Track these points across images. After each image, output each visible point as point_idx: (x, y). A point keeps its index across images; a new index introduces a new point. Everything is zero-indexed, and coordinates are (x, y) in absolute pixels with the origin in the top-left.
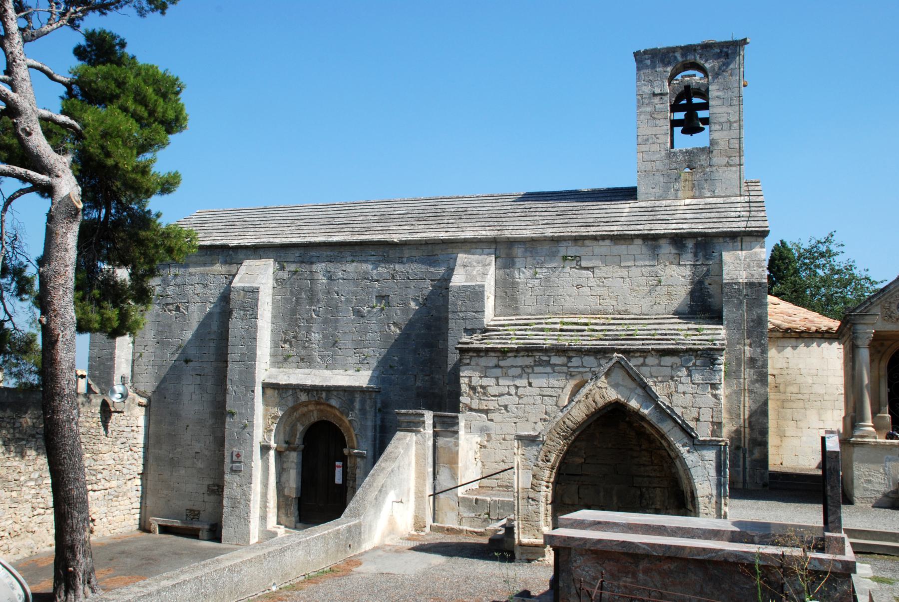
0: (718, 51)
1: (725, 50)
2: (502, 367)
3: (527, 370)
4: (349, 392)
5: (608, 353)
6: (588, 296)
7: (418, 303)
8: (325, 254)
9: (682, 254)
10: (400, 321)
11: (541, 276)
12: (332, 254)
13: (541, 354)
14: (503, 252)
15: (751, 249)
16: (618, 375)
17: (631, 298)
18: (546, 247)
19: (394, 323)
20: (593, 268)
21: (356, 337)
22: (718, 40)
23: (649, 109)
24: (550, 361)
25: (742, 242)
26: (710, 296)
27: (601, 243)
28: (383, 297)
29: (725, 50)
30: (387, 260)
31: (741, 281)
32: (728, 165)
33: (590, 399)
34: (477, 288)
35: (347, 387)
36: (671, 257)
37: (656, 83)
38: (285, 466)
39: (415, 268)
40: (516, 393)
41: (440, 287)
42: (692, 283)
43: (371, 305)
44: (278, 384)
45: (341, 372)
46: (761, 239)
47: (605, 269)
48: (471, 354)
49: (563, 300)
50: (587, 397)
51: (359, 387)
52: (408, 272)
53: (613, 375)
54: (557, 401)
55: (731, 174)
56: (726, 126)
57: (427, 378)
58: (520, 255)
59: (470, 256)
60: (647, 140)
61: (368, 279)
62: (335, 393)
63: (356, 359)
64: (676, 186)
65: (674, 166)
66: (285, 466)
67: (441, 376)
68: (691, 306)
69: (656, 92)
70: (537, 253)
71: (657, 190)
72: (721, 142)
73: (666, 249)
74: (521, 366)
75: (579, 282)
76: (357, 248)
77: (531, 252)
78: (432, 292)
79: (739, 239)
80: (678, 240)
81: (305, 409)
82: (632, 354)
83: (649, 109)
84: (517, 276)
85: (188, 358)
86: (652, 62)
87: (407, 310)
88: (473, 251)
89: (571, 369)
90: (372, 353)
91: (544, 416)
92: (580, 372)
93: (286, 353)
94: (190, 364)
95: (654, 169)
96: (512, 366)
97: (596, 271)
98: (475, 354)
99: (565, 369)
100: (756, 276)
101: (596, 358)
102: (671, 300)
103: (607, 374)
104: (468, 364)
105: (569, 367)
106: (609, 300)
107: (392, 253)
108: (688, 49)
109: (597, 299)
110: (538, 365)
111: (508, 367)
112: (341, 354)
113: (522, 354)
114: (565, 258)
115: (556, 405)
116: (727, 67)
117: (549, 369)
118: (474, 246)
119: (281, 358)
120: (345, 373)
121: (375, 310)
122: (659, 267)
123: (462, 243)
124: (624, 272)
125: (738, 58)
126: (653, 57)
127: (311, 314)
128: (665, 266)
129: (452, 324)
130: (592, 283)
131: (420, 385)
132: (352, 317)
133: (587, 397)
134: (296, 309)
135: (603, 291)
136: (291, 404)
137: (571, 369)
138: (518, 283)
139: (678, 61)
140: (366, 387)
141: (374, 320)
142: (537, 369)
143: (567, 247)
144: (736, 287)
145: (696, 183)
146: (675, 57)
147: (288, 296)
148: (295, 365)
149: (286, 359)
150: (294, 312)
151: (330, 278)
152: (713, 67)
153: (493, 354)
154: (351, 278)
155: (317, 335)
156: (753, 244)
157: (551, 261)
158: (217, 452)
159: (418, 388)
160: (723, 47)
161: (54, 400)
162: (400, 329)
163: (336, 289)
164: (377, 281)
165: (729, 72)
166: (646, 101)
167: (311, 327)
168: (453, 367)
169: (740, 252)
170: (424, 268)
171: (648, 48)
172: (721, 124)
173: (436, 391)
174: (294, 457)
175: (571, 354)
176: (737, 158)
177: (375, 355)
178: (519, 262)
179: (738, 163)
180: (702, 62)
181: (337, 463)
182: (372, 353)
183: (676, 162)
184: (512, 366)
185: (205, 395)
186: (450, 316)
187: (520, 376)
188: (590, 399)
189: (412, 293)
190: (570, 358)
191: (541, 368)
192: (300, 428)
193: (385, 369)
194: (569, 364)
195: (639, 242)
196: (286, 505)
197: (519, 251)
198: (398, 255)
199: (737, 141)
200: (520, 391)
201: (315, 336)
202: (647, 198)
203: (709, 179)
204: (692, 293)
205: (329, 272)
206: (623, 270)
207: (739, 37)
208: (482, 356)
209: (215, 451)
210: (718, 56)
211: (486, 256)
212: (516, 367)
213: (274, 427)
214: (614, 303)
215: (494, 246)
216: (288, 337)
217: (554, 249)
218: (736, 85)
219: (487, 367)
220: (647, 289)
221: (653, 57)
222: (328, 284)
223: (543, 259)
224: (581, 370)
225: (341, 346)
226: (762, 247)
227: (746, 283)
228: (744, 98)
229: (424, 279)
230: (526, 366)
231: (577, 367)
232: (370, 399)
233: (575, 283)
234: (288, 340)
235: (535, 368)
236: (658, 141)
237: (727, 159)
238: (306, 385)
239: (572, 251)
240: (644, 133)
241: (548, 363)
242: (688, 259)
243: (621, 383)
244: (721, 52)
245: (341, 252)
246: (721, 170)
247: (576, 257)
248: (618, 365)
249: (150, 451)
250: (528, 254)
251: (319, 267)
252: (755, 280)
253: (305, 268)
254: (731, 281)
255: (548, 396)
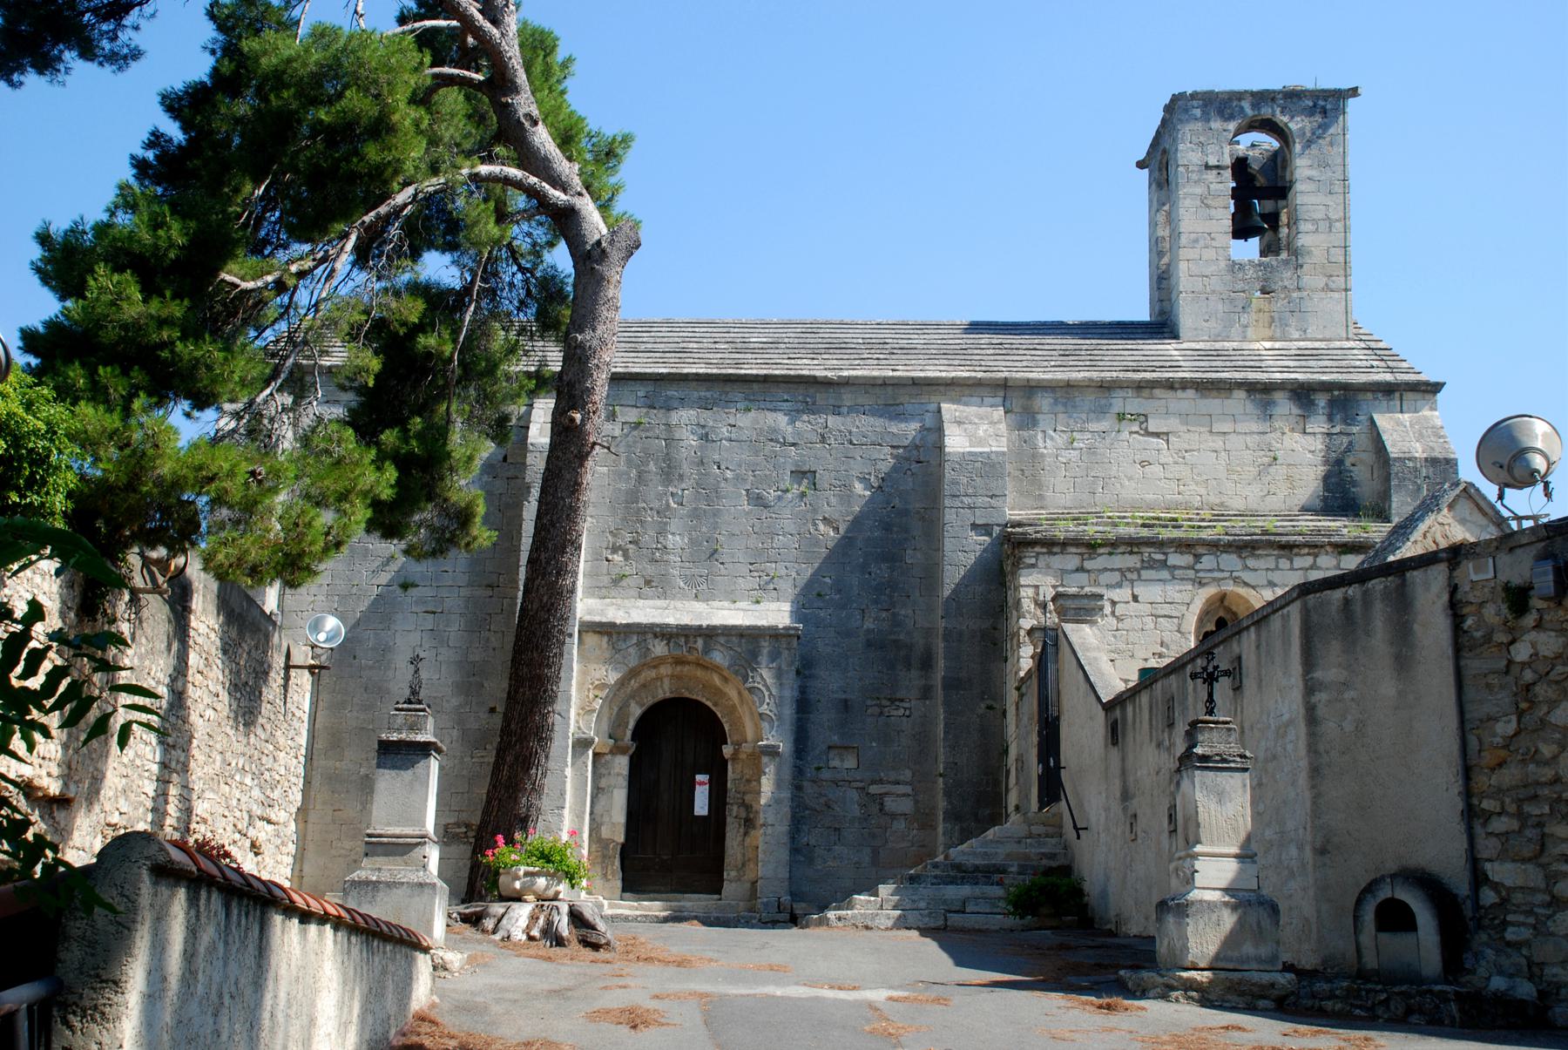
0: (1311, 104)
1: (1321, 103)
2: (1088, 571)
3: (1129, 575)
4: (749, 639)
5: (1259, 549)
6: (1160, 480)
7: (869, 486)
8: (696, 394)
9: (1309, 416)
10: (836, 516)
11: (1082, 445)
12: (708, 394)
13: (1152, 550)
14: (1017, 403)
15: (1416, 411)
16: (1465, 507)
17: (1230, 484)
18: (1090, 398)
19: (825, 519)
20: (1167, 434)
21: (754, 542)
22: (1310, 86)
23: (1199, 190)
24: (1166, 561)
25: (1401, 400)
26: (1354, 483)
27: (1180, 393)
28: (804, 473)
29: (1321, 103)
30: (812, 409)
31: (1417, 455)
32: (1327, 289)
33: (1429, 539)
34: (993, 456)
35: (749, 628)
36: (1293, 419)
37: (1210, 149)
38: (603, 783)
39: (866, 425)
40: (1113, 613)
41: (907, 459)
42: (1326, 462)
43: (782, 487)
44: (612, 625)
45: (726, 604)
46: (1431, 396)
47: (1187, 436)
48: (1038, 549)
49: (1118, 485)
50: (1425, 536)
51: (770, 628)
52: (850, 432)
53: (1458, 507)
54: (1180, 625)
55: (1333, 303)
56: (1323, 226)
57: (884, 615)
58: (1045, 408)
59: (961, 408)
60: (1196, 241)
61: (778, 442)
62: (722, 640)
63: (753, 582)
64: (1244, 319)
65: (1240, 286)
66: (603, 783)
67: (910, 611)
68: (1325, 499)
69: (1210, 164)
70: (1074, 407)
71: (1212, 324)
72: (1316, 252)
73: (1284, 406)
74: (1119, 570)
75: (1145, 456)
76: (755, 386)
77: (1065, 405)
78: (894, 469)
79: (1397, 395)
80: (1303, 394)
81: (653, 674)
82: (1296, 550)
83: (1199, 190)
84: (1041, 444)
85: (410, 580)
86: (1203, 112)
87: (849, 496)
88: (964, 399)
89: (1201, 574)
90: (783, 572)
91: (1159, 649)
92: (1214, 579)
93: (617, 570)
94: (412, 591)
95: (1208, 290)
96: (1106, 570)
97: (1172, 438)
98: (1044, 550)
99: (1191, 573)
100: (1438, 450)
101: (1240, 557)
102: (1293, 488)
103: (1451, 507)
104: (1033, 566)
105: (1197, 571)
106: (1194, 487)
107: (821, 398)
108: (1262, 97)
109: (1174, 485)
110: (1147, 568)
111: (1099, 571)
112: (723, 572)
113: (1121, 549)
114: (1121, 417)
115: (1179, 631)
116: (1325, 131)
117: (1165, 574)
118: (967, 392)
119: (606, 580)
120: (732, 606)
121: (789, 495)
122: (1272, 435)
123: (947, 385)
124: (1218, 443)
125: (1341, 118)
126: (1206, 106)
127: (667, 501)
128: (1283, 434)
129: (949, 516)
130: (1166, 457)
131: (872, 626)
132: (747, 508)
133: (1425, 536)
134: (638, 491)
135: (1185, 472)
136: (633, 662)
137: (1201, 574)
138: (1043, 455)
139: (1246, 115)
140: (784, 628)
141: (787, 513)
142: (1145, 574)
143: (1125, 398)
144: (1411, 464)
145: (1276, 315)
146: (1242, 108)
147: (623, 467)
148: (634, 592)
149: (617, 581)
150: (633, 497)
151: (705, 437)
152: (1302, 130)
153: (1073, 550)
154: (745, 438)
155: (678, 538)
156: (1419, 403)
157: (1098, 420)
158: (467, 759)
159: (868, 631)
160: (1318, 98)
161: (564, 552)
162: (836, 529)
163: (716, 457)
164: (794, 445)
165: (1328, 139)
166: (1194, 176)
167: (666, 524)
168: (954, 591)
169: (1400, 416)
170: (878, 423)
171: (1199, 90)
172: (1315, 222)
173: (902, 637)
174: (622, 764)
175: (1200, 550)
176: (1342, 279)
177: (793, 573)
178: (1044, 420)
179: (1343, 287)
180: (1285, 119)
181: (699, 778)
182: (783, 572)
183: (1243, 280)
184: (1106, 570)
185: (443, 650)
186: (947, 502)
187: (1119, 585)
188: (1429, 539)
189: (857, 467)
190: (1197, 557)
191: (1153, 572)
192: (636, 711)
193: (808, 601)
194: (1198, 567)
195: (1240, 394)
196: (604, 856)
197: (1043, 402)
198: (831, 401)
199: (1341, 252)
200: (1119, 609)
201: (675, 541)
202: (1197, 335)
203: (1296, 310)
204: (1326, 478)
205: (703, 427)
206: (1215, 438)
207: (1345, 86)
208: (1056, 554)
209: (462, 758)
210: (1311, 112)
211: (989, 409)
212: (1112, 570)
213: (597, 704)
214: (1203, 491)
215: (1002, 394)
216: (619, 542)
217: (1103, 402)
218: (1339, 160)
219: (1064, 572)
220: (1254, 471)
221: (1206, 106)
222: (701, 447)
223: (1084, 416)
224: (1217, 575)
225: (724, 558)
226: (1432, 409)
227: (1426, 459)
228: (1352, 182)
229: (880, 445)
230: (1129, 569)
231: (1210, 571)
232: (789, 649)
233: (1138, 458)
234: (620, 548)
235: (1143, 572)
236: (1214, 243)
237: (1325, 279)
238: (668, 625)
239: (1134, 404)
240: (1191, 229)
241: (1164, 564)
242: (1319, 425)
243: (1468, 518)
244: (1315, 106)
245: (727, 393)
246: (1316, 297)
247: (1139, 415)
248: (1464, 494)
249: (315, 763)
250: (1060, 408)
251: (685, 416)
252: (1436, 454)
253: (657, 417)
254: (1401, 455)
255: (1165, 616)
